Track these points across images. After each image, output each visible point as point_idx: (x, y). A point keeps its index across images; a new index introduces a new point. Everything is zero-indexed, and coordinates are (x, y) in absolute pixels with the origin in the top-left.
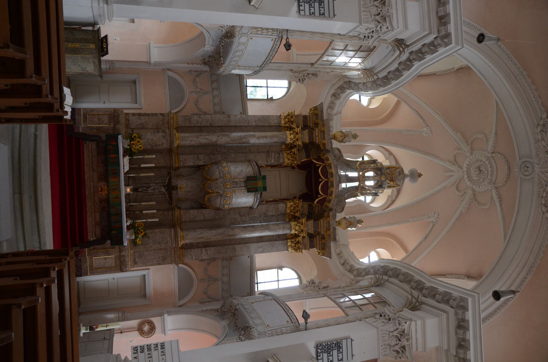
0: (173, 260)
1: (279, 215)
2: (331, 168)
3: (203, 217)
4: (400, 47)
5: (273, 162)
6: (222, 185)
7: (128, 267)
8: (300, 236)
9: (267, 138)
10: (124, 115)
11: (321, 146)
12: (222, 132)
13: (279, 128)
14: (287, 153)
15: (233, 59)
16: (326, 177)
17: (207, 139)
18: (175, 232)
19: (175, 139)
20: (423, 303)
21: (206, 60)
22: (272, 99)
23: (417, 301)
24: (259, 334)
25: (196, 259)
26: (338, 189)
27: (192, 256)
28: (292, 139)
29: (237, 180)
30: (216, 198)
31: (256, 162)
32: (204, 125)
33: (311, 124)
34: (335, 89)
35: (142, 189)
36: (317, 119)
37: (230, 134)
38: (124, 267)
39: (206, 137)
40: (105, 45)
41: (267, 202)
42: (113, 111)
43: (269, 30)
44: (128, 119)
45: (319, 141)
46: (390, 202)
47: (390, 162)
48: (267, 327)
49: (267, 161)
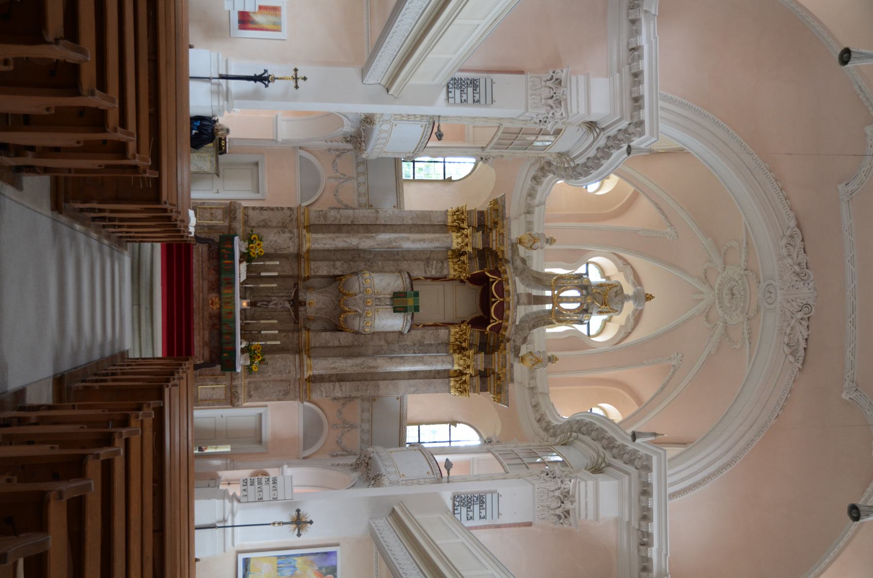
0: (298, 395)
1: (439, 344)
2: (508, 284)
3: (338, 343)
5: (433, 273)
6: (362, 302)
9: (425, 242)
10: (242, 209)
11: (499, 254)
12: (368, 233)
13: (444, 228)
16: (502, 296)
17: (346, 242)
18: (300, 360)
19: (304, 242)
20: (609, 465)
23: (604, 461)
25: (326, 397)
28: (460, 244)
29: (381, 296)
30: (354, 319)
33: (489, 223)
35: (262, 303)
38: (235, 400)
41: (424, 326)
45: (496, 247)
46: (622, 335)
49: (425, 272)
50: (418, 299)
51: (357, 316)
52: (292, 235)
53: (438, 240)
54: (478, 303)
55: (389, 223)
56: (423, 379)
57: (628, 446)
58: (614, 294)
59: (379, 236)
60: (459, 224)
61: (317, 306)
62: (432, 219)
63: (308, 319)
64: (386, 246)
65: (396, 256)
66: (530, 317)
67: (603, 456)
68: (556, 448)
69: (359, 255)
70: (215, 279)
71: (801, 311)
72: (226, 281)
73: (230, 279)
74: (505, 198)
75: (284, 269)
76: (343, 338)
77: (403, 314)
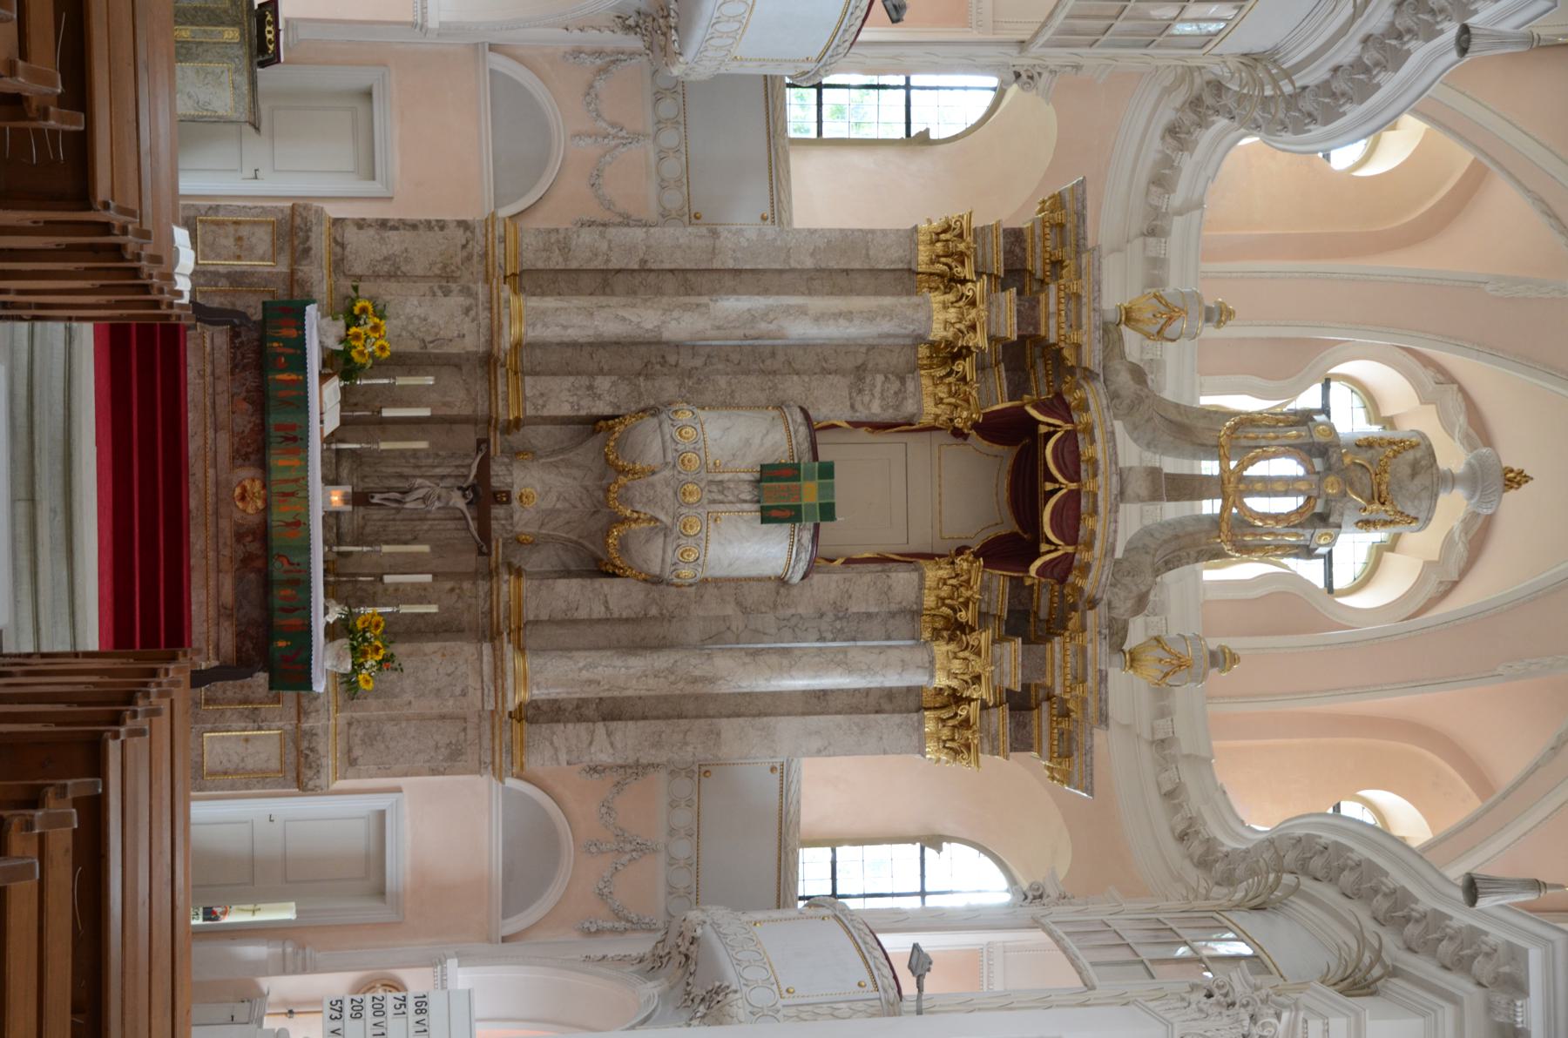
0: (488, 760)
1: (893, 615)
2: (1093, 441)
3: (603, 609)
5: (875, 409)
6: (670, 494)
7: (323, 776)
9: (851, 320)
10: (326, 225)
11: (1066, 353)
12: (687, 294)
13: (906, 278)
14: (933, 377)
16: (1074, 476)
17: (624, 319)
18: (495, 656)
19: (505, 320)
20: (1394, 972)
23: (1378, 957)
24: (752, 1013)
25: (568, 763)
28: (953, 324)
29: (726, 476)
30: (647, 541)
31: (802, 409)
32: (617, 267)
33: (1039, 264)
34: (1177, 110)
35: (386, 495)
37: (712, 305)
38: (310, 773)
39: (621, 313)
41: (849, 561)
42: (289, 212)
44: (339, 239)
45: (1059, 335)
46: (1430, 589)
48: (785, 994)
49: (852, 407)
50: (832, 486)
51: (657, 533)
52: (469, 301)
53: (888, 314)
54: (1005, 494)
55: (748, 267)
56: (846, 713)
57: (1451, 918)
58: (1408, 471)
60: (950, 268)
61: (545, 505)
62: (871, 253)
65: (768, 362)
66: (1157, 535)
67: (1358, 927)
68: (1234, 917)
69: (663, 357)
72: (282, 433)
73: (293, 427)
74: (1084, 191)
75: (448, 399)
76: (618, 595)
77: (787, 527)
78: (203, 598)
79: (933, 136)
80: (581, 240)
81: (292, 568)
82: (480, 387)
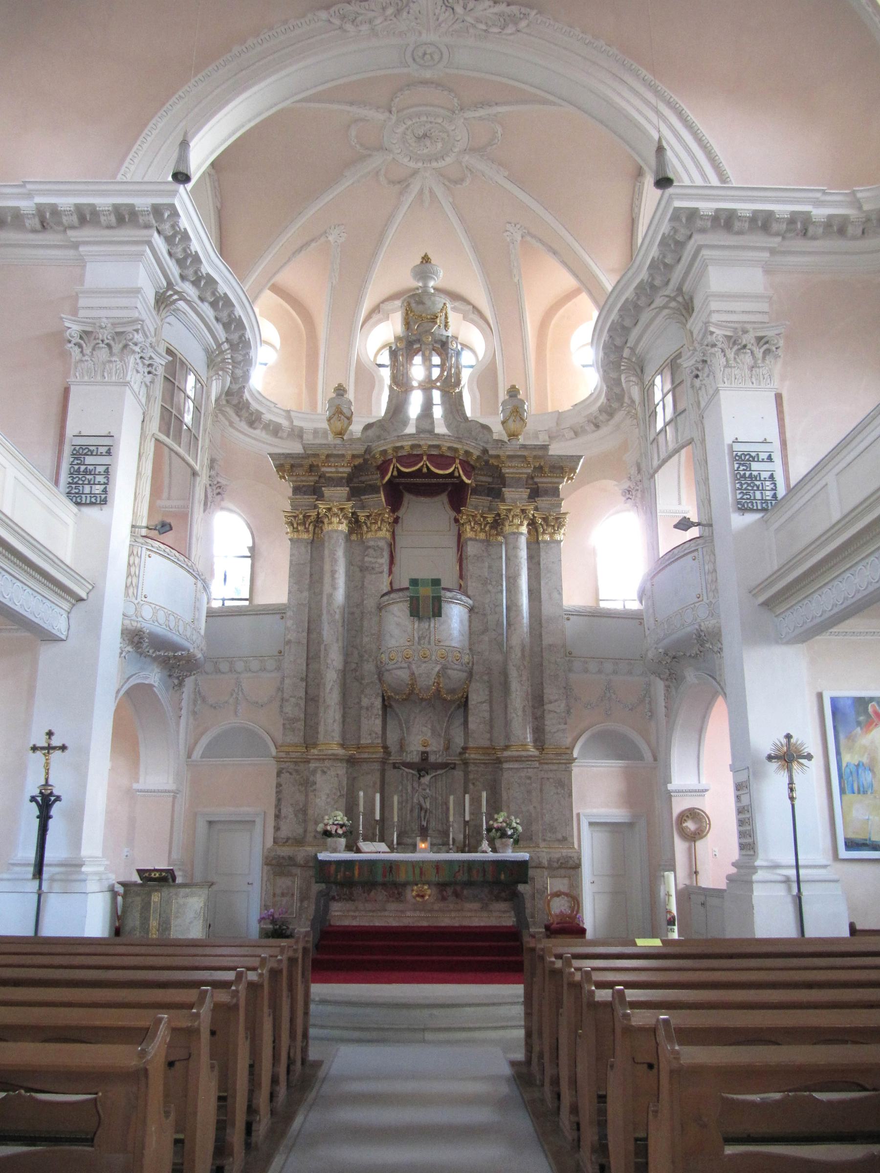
0: (564, 766)
2: (402, 447)
4: (171, 300)
5: (385, 560)
6: (424, 665)
8: (533, 515)
14: (367, 532)
15: (181, 632)
16: (419, 457)
17: (331, 689)
18: (509, 761)
20: (680, 290)
21: (176, 682)
22: (252, 549)
25: (565, 724)
26: (444, 435)
27: (558, 731)
28: (340, 520)
33: (311, 478)
34: (241, 420)
35: (423, 819)
36: (301, 466)
38: (571, 862)
40: (155, 875)
42: (269, 868)
43: (131, 562)
44: (284, 840)
45: (347, 466)
46: (476, 317)
47: (394, 311)
50: (422, 579)
51: (446, 673)
59: (325, 638)
61: (429, 734)
63: (447, 748)
64: (340, 629)
67: (657, 310)
70: (383, 891)
71: (453, 9)
72: (388, 874)
78: (477, 919)
79: (251, 545)
80: (290, 712)
81: (461, 872)
82: (365, 767)
